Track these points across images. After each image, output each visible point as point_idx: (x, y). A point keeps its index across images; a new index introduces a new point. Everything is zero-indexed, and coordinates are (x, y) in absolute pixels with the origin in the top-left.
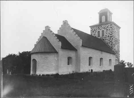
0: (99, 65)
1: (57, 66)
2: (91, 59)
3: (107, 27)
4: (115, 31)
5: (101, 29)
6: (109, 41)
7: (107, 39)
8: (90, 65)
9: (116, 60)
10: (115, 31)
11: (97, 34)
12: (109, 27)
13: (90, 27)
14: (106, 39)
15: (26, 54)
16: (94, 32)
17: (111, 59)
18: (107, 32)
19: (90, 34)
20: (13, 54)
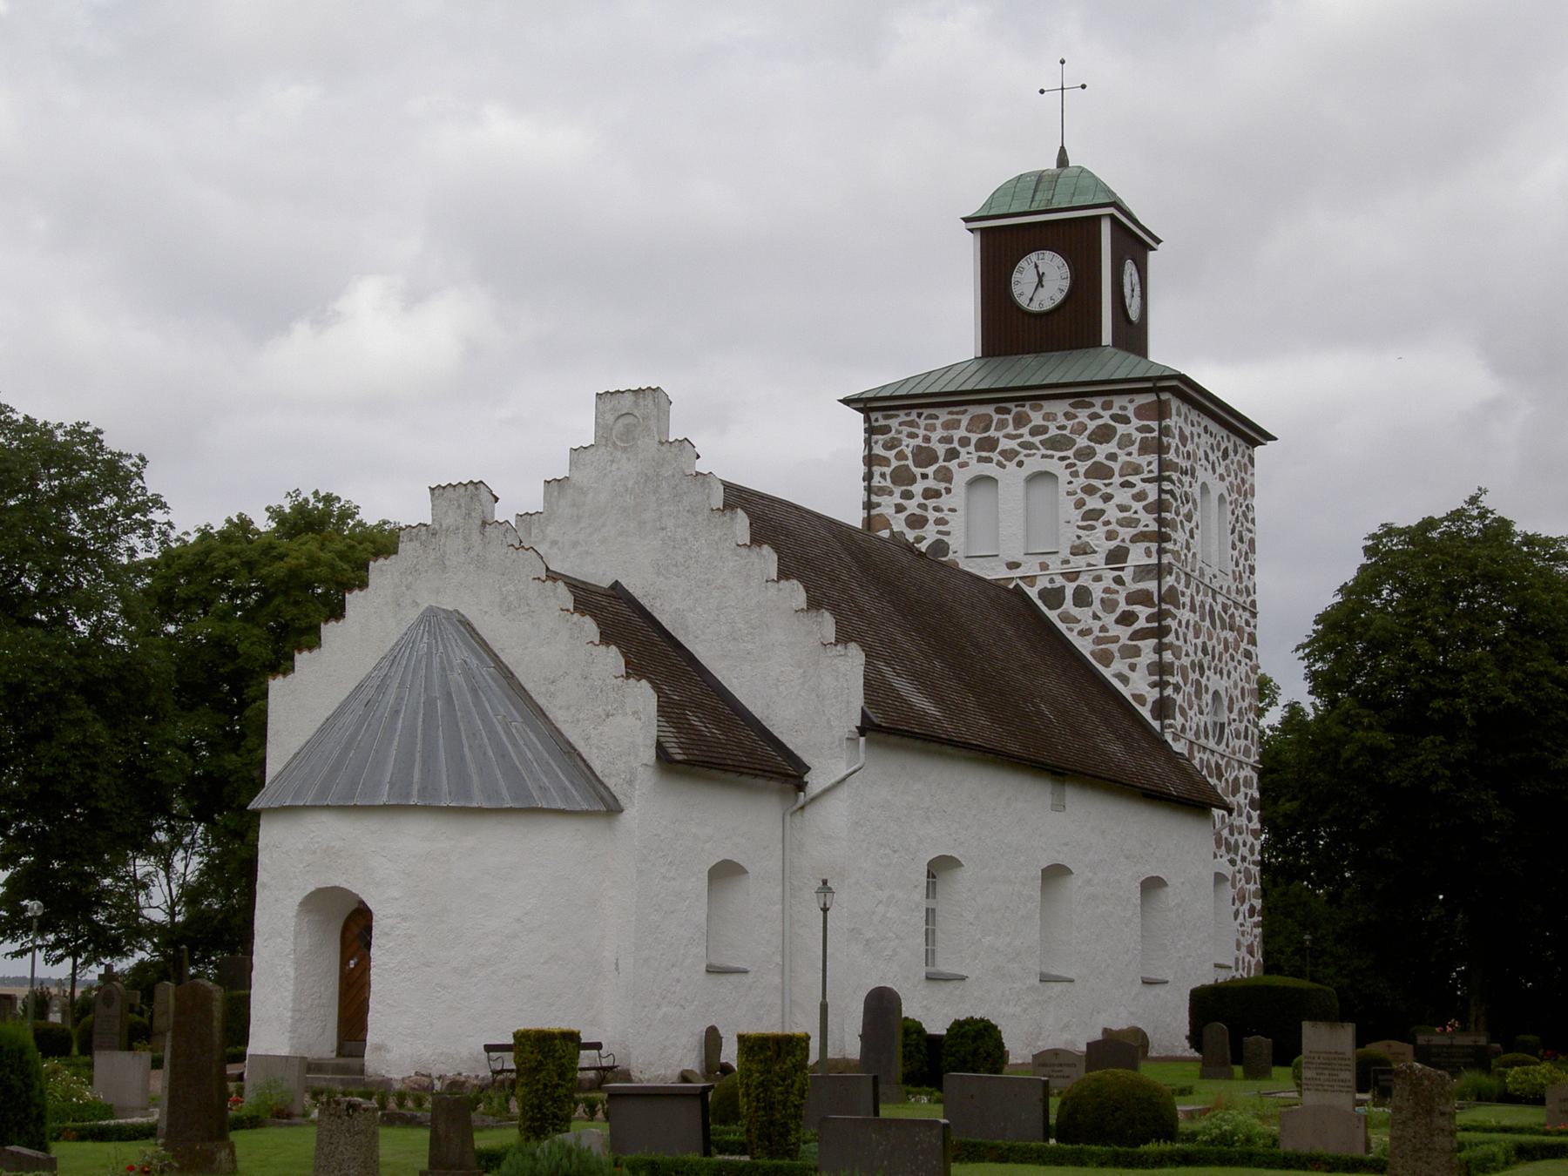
0: (1167, 987)
1: (1479, 1099)
2: (939, 881)
3: (1104, 435)
4: (1196, 490)
5: (1009, 455)
6: (1126, 619)
7: (1097, 591)
8: (746, 972)
9: (1219, 878)
10: (1196, 490)
11: (1240, 450)
12: (1121, 429)
13: (864, 404)
14: (1082, 597)
15: (235, 742)
16: (918, 488)
17: (1062, 859)
18: (1094, 503)
19: (853, 517)
20: (263, 523)
